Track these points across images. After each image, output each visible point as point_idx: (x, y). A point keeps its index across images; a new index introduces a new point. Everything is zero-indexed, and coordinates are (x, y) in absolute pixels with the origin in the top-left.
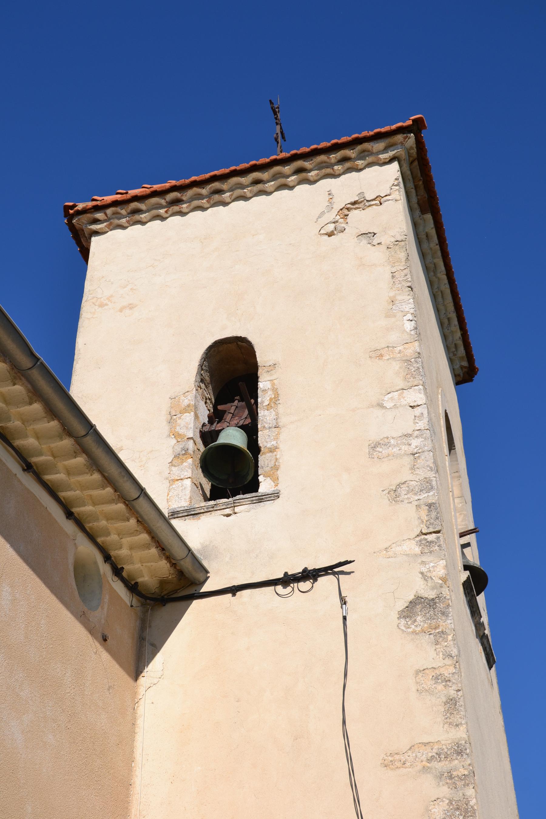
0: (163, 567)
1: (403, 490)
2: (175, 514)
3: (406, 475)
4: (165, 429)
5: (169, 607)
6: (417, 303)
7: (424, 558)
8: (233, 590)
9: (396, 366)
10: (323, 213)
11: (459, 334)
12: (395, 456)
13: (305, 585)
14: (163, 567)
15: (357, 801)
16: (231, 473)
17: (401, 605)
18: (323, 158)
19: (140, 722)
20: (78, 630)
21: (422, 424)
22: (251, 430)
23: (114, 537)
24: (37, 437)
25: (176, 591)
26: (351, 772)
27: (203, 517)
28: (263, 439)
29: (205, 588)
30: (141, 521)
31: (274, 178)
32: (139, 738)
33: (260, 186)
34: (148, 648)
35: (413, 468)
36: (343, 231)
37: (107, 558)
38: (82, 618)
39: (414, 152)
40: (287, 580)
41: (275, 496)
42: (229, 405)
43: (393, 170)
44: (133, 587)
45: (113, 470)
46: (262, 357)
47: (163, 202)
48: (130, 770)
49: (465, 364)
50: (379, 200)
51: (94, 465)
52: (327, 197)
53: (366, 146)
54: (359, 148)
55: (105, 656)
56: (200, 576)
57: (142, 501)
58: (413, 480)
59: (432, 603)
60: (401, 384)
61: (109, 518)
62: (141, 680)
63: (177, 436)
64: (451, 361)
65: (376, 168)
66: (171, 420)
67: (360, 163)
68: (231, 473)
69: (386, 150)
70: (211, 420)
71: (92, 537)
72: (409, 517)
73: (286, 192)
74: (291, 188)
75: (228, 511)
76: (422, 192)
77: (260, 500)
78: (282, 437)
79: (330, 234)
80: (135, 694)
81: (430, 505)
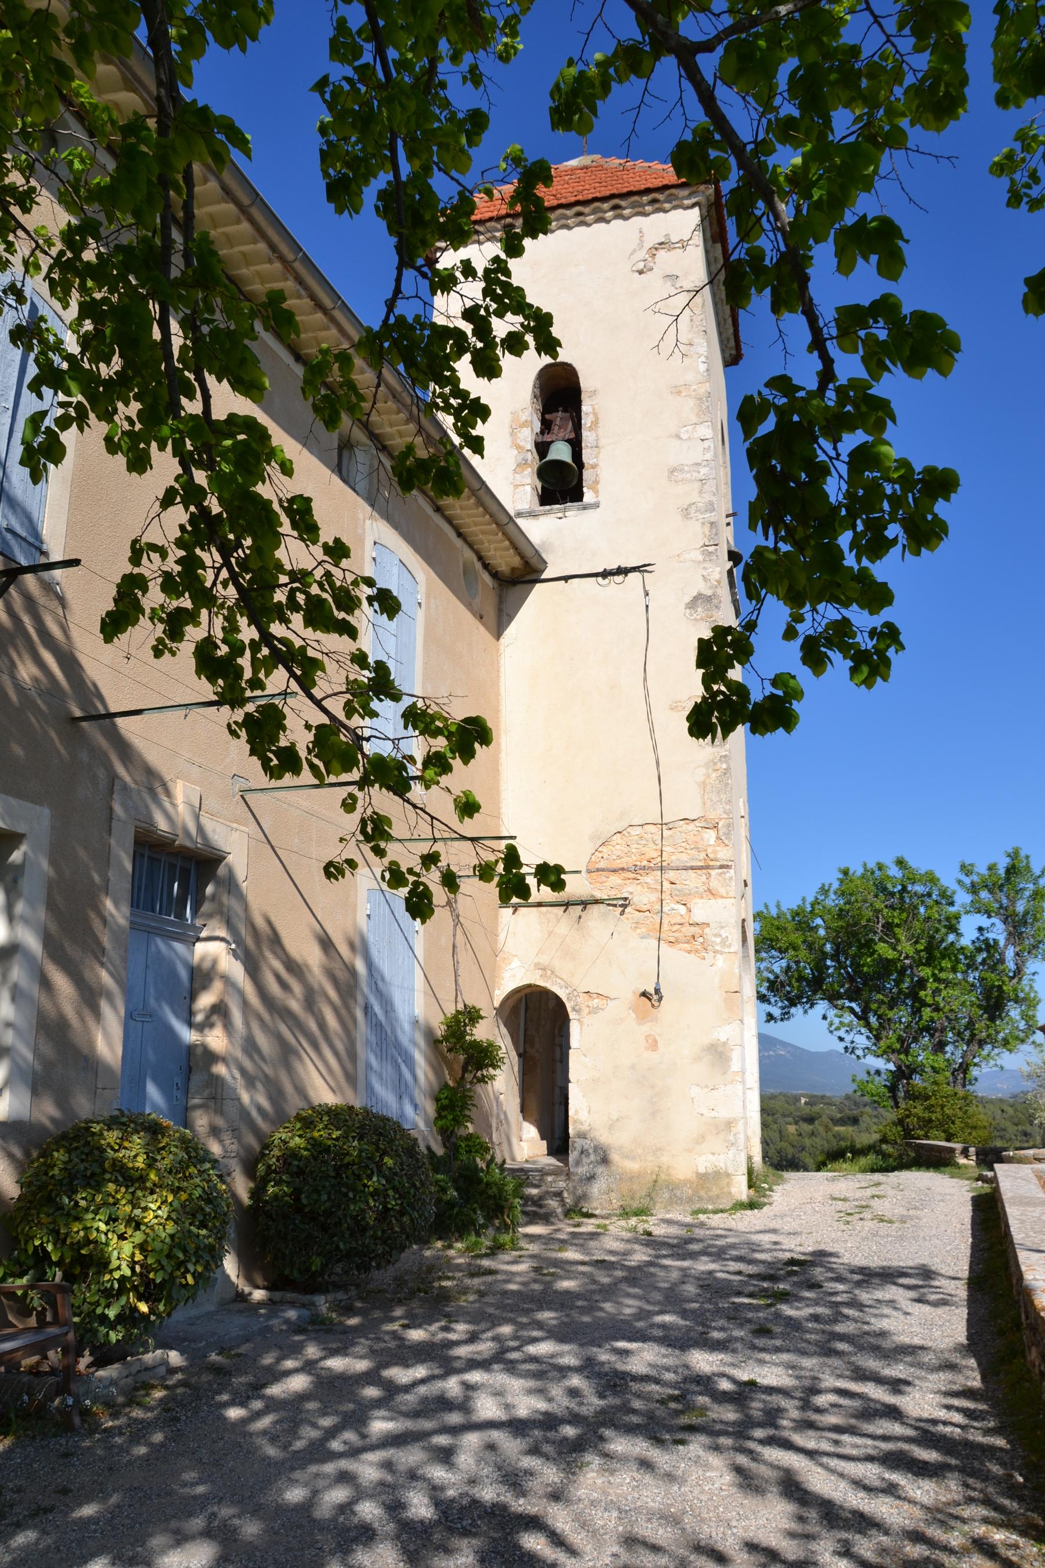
0: (516, 561)
1: (693, 509)
2: (519, 514)
3: (695, 497)
4: (509, 440)
5: (519, 587)
6: (709, 346)
7: (706, 565)
8: (566, 578)
9: (691, 402)
10: (634, 251)
11: (731, 331)
12: (689, 481)
13: (619, 579)
14: (516, 561)
15: (652, 731)
16: (561, 485)
17: (688, 599)
18: (636, 198)
19: (502, 669)
20: (468, 615)
21: (709, 456)
22: (576, 445)
23: (492, 552)
24: (462, 508)
25: (523, 576)
26: (649, 712)
27: (541, 518)
28: (587, 456)
29: (544, 576)
30: (486, 509)
31: (594, 212)
32: (502, 680)
33: (581, 218)
34: (505, 618)
35: (701, 492)
36: (651, 269)
37: (480, 558)
38: (469, 606)
39: (712, 198)
40: (605, 574)
41: (596, 506)
42: (554, 414)
43: (694, 215)
44: (495, 575)
45: (494, 508)
46: (586, 383)
47: (499, 226)
48: (498, 701)
49: (734, 352)
50: (683, 245)
51: (480, 503)
52: (638, 235)
53: (673, 191)
54: (667, 192)
55: (482, 629)
56: (542, 567)
57: (510, 525)
58: (701, 501)
59: (709, 599)
60: (695, 420)
61: (483, 533)
62: (502, 640)
63: (518, 447)
64: (723, 351)
65: (680, 211)
66: (513, 434)
67: (667, 206)
68: (561, 485)
69: (689, 197)
70: (542, 432)
71: (471, 546)
72: (695, 532)
73: (603, 225)
74: (608, 222)
75: (560, 515)
76: (715, 227)
77: (585, 508)
78: (601, 456)
79: (641, 272)
80: (498, 650)
81: (712, 524)
